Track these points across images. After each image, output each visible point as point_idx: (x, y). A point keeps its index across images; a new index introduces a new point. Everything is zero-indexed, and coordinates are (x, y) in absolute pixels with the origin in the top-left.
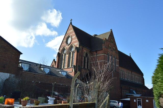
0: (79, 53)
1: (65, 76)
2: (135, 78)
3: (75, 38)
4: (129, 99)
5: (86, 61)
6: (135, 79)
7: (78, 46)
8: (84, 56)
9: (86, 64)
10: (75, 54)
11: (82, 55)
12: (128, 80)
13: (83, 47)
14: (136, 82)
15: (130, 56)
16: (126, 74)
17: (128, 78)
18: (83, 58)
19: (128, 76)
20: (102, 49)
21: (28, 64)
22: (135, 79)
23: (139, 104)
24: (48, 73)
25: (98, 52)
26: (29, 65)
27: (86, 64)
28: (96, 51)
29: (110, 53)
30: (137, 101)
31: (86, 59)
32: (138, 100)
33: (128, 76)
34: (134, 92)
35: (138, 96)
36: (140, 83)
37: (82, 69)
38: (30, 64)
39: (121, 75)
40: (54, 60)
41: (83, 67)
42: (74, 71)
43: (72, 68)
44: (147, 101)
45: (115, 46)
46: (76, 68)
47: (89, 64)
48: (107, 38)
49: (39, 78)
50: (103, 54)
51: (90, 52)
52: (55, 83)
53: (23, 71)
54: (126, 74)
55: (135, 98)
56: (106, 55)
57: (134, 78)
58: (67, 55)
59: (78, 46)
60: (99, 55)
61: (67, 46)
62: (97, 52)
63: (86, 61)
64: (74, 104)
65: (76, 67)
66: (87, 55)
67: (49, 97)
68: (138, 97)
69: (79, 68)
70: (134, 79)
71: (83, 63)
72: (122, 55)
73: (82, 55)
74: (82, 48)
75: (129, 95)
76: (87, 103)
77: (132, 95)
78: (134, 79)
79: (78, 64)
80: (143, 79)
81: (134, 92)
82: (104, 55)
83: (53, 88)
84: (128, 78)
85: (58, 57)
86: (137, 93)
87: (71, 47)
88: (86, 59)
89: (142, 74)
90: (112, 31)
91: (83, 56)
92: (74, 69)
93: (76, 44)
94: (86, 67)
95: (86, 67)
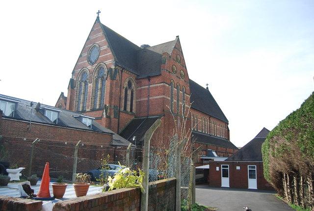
0: (115, 81)
1: (90, 126)
2: (215, 128)
3: (106, 50)
4: (207, 167)
5: (129, 97)
6: (215, 130)
7: (113, 67)
8: (125, 86)
9: (129, 103)
10: (108, 83)
11: (121, 85)
12: (204, 132)
13: (123, 69)
14: (217, 136)
15: (207, 88)
16: (202, 123)
17: (203, 128)
18: (124, 91)
19: (204, 126)
20: (160, 75)
21: (13, 102)
22: (215, 130)
23: (225, 175)
24: (55, 121)
25: (152, 80)
26: (14, 104)
27: (129, 103)
28: (149, 78)
29: (175, 82)
30: (222, 168)
31: (129, 92)
32: (223, 167)
33: (204, 126)
34: (214, 153)
35: (222, 159)
36: (223, 137)
37: (121, 113)
38: (16, 103)
39: (192, 123)
40: (62, 93)
41: (122, 109)
42: (105, 116)
43: (102, 111)
44: (238, 168)
45: (184, 68)
46: (109, 111)
47: (134, 103)
48: (170, 53)
49: (37, 132)
50: (162, 84)
51: (137, 79)
52: (80, 145)
53: (3, 117)
54: (202, 123)
55: (218, 164)
56: (167, 85)
57: (216, 128)
58: (89, 85)
59: (113, 67)
60: (155, 85)
61: (90, 66)
62: (149, 80)
63: (129, 97)
64: (151, 183)
65: (110, 109)
66: (130, 84)
67: (8, 170)
68: (222, 163)
69: (115, 112)
70: (206, 129)
71: (123, 101)
72: (194, 86)
73: (121, 85)
74: (122, 71)
75: (206, 159)
76: (166, 182)
77: (211, 159)
78: (213, 131)
79: (113, 103)
80: (228, 130)
81: (214, 153)
82: (164, 86)
83: (76, 152)
84: (203, 128)
85: (70, 88)
86: (219, 156)
87: (100, 68)
88: (129, 92)
89: (226, 122)
90: (179, 38)
91: (124, 88)
92: (104, 113)
93: (110, 62)
94: (128, 109)
95: (128, 109)
